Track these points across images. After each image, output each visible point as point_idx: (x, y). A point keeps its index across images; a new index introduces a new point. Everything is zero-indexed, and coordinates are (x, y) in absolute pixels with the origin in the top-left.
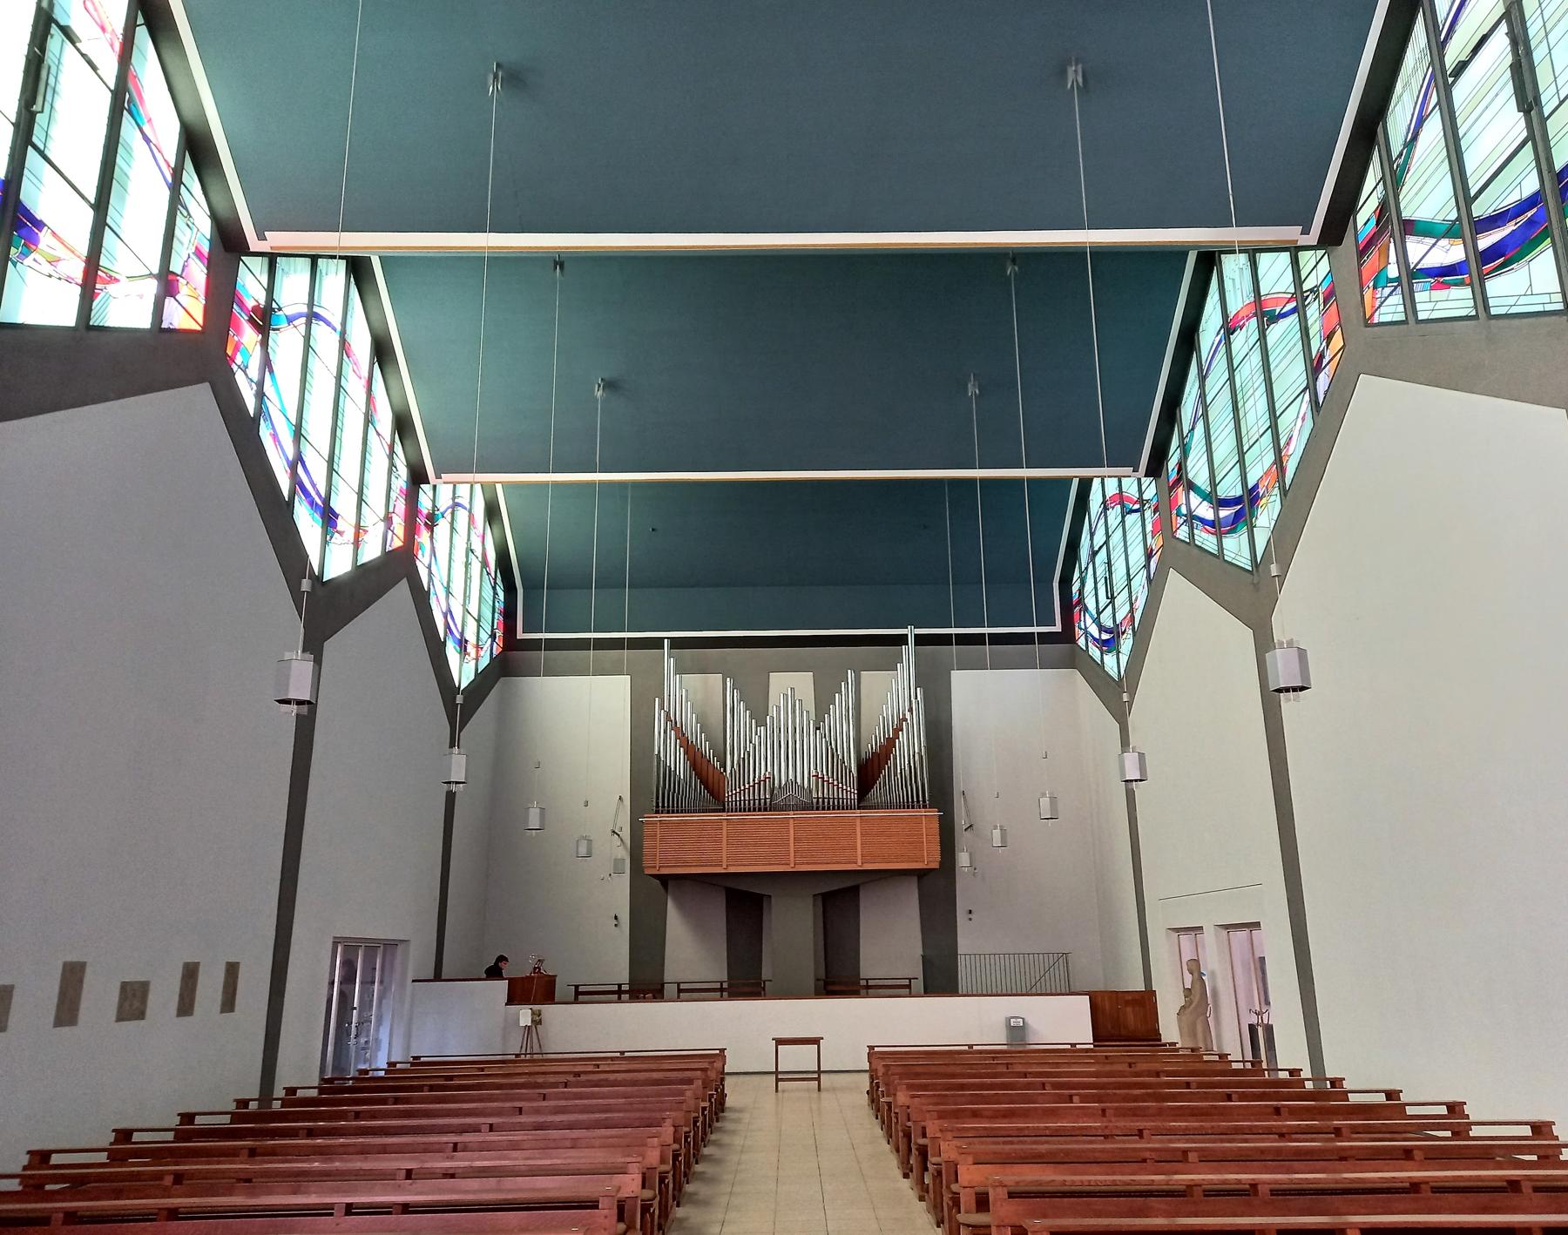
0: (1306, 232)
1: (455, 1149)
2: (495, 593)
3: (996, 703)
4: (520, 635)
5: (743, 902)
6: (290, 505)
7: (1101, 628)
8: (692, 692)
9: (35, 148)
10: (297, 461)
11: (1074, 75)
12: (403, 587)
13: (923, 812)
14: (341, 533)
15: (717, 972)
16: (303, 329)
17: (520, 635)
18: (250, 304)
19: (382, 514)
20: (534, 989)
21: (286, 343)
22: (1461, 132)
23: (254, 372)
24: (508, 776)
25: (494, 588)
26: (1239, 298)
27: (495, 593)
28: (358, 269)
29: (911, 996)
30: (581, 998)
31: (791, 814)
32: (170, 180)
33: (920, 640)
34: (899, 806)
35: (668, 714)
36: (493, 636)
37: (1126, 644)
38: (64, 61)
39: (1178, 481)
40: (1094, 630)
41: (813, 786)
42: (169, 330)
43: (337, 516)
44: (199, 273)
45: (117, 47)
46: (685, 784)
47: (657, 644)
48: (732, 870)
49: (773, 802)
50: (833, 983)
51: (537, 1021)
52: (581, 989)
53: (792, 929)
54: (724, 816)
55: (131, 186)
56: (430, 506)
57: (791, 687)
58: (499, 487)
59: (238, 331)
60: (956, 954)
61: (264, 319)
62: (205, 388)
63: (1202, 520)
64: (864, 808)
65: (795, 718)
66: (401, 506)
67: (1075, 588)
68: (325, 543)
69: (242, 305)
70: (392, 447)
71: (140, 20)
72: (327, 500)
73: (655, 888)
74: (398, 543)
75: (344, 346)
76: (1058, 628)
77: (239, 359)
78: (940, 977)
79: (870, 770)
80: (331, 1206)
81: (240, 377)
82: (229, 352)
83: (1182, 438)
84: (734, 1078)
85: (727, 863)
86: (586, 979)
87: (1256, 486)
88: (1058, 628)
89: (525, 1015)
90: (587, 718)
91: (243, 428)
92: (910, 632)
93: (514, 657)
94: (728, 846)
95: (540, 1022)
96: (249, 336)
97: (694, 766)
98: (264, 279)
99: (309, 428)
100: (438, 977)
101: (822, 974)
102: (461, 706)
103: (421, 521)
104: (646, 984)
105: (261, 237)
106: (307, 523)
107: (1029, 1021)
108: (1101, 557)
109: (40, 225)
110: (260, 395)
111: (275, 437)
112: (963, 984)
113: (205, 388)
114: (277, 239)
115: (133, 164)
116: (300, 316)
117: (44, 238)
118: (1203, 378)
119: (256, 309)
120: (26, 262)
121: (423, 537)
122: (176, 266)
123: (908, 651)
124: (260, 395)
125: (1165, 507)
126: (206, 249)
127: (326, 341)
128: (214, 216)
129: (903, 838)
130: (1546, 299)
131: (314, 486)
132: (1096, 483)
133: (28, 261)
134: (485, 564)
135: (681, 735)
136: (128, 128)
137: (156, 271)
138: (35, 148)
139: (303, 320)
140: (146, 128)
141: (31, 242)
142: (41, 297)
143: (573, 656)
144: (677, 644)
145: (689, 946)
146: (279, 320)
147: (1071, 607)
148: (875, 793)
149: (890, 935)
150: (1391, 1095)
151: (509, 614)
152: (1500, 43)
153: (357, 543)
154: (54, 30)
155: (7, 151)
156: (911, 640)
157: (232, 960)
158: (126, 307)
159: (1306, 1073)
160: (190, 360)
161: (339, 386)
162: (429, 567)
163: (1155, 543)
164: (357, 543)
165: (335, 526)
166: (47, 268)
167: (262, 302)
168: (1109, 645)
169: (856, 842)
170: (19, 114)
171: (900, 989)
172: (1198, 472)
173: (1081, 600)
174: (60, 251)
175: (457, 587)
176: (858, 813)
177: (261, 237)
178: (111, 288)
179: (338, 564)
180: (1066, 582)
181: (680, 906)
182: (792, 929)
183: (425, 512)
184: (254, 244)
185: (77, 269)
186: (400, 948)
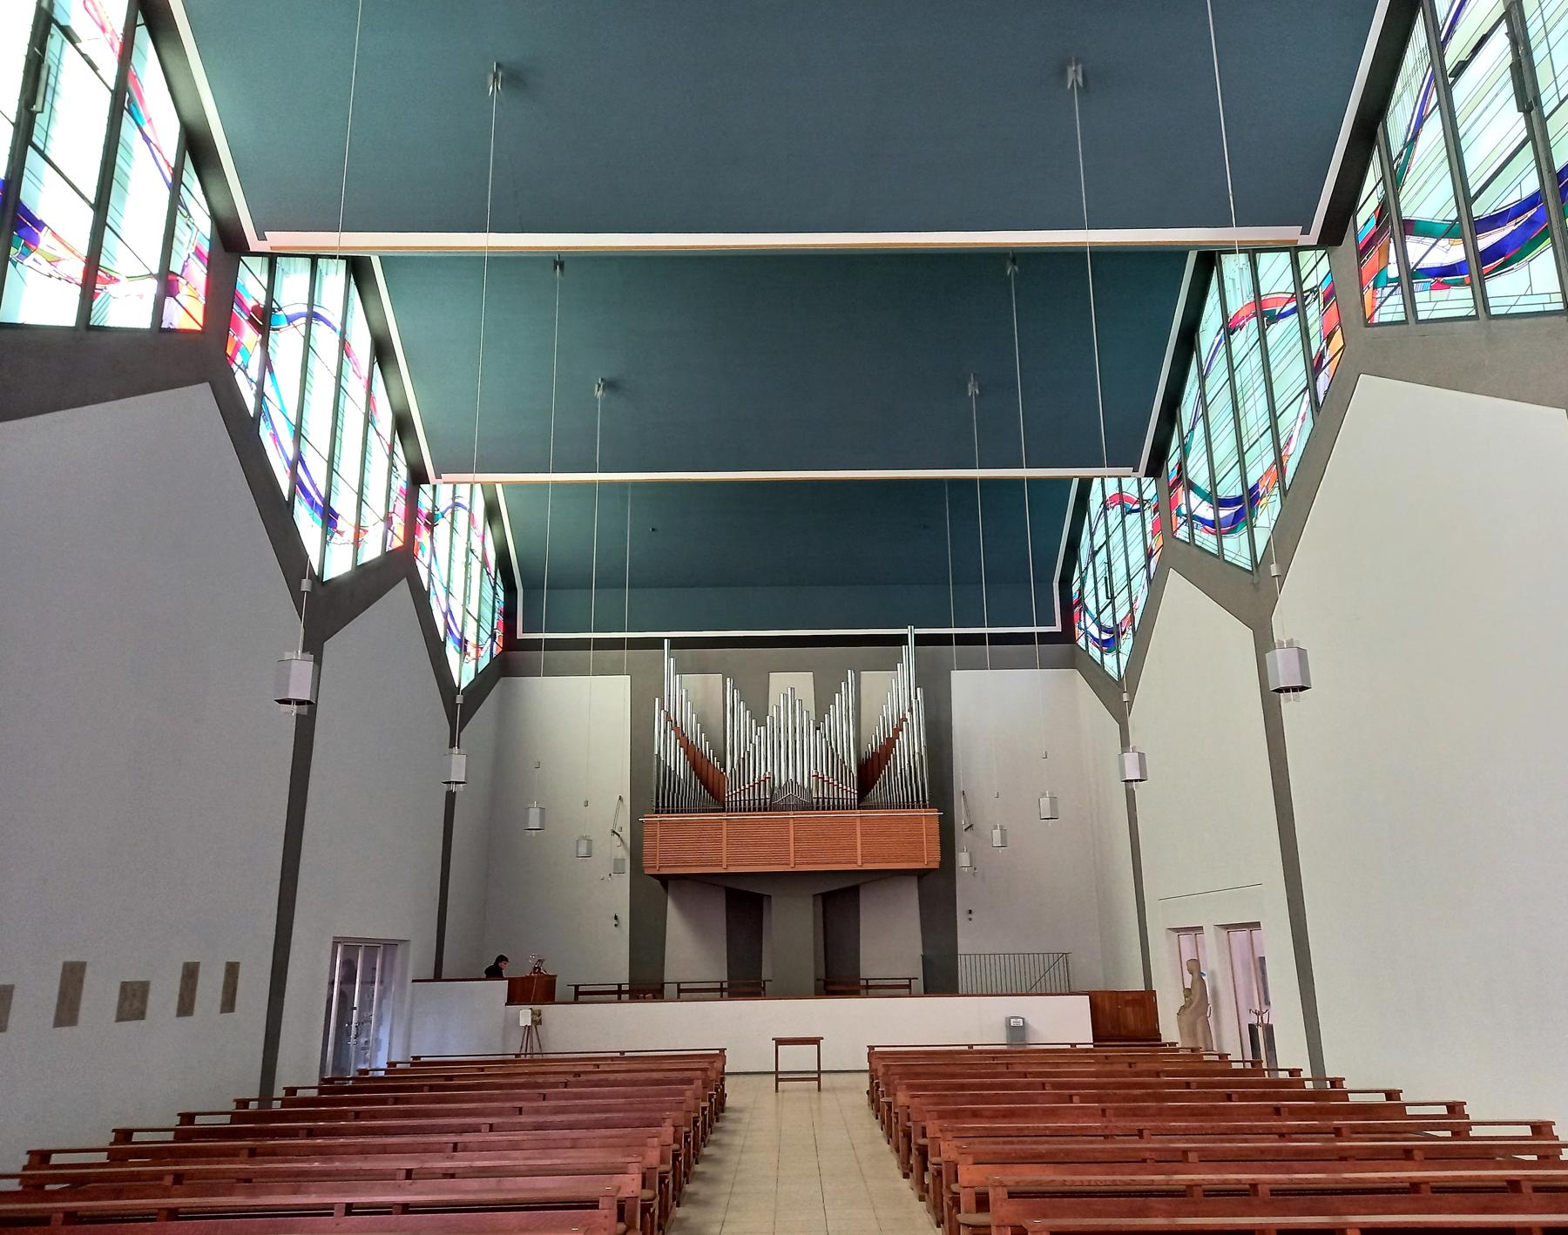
0: (1306, 232)
1: (455, 1149)
2: (495, 593)
3: (996, 703)
4: (520, 635)
5: (743, 902)
6: (290, 505)
7: (1101, 628)
8: (692, 692)
9: (35, 148)
10: (297, 461)
11: (1074, 75)
12: (403, 587)
13: (923, 812)
14: (341, 533)
15: (717, 972)
16: (303, 329)
17: (520, 635)
18: (250, 304)
19: (382, 514)
20: (534, 989)
21: (286, 343)
22: (1461, 132)
23: (254, 372)
24: (508, 776)
25: (494, 588)
26: (1239, 298)
27: (495, 593)
28: (358, 269)
29: (911, 996)
30: (581, 998)
31: (791, 814)
32: (170, 180)
33: (920, 640)
34: (899, 806)
35: (668, 714)
36: (493, 636)
37: (1126, 644)
38: (64, 61)
39: (1178, 481)
40: (1094, 630)
41: (813, 786)
42: (169, 330)
43: (337, 516)
44: (199, 273)
45: (117, 47)
47: (657, 644)
48: (732, 870)
49: (773, 802)
50: (833, 983)
51: (537, 1021)
52: (581, 989)
53: (792, 929)
54: (724, 816)
55: (131, 186)
56: (430, 506)
57: (791, 687)
58: (499, 487)
59: (238, 331)
60: (956, 954)
61: (264, 319)
62: (205, 388)
63: (1202, 520)
64: (864, 808)
65: (795, 718)
66: (401, 506)
67: (1075, 588)
68: (325, 543)
69: (242, 305)
70: (392, 447)
71: (140, 20)
72: (327, 500)
73: (655, 888)
74: (398, 543)
75: (344, 346)
76: (1058, 628)
77: (239, 359)
78: (940, 977)
79: (870, 770)
80: (331, 1206)
81: (240, 377)
82: (229, 352)
83: (1182, 438)
84: (734, 1078)
85: (727, 863)
86: (586, 979)
87: (1256, 486)
88: (1058, 628)
89: (525, 1015)
90: (587, 718)
91: (243, 428)
92: (910, 632)
93: (514, 657)
94: (728, 846)
95: (540, 1022)
96: (249, 336)
97: (694, 766)
98: (264, 279)
99: (309, 428)
100: (438, 977)
101: (822, 974)
102: (461, 706)
103: (421, 521)
104: (646, 984)
105: (261, 237)
106: (307, 523)
107: (1029, 1021)
108: (1101, 557)
109: (40, 225)
110: (260, 395)
111: (275, 437)
112: (963, 984)
113: (205, 388)
114: (277, 239)
115: (133, 164)
116: (300, 316)
117: (44, 238)
118: (1203, 378)
119: (256, 309)
120: (26, 262)
121: (423, 537)
122: (176, 266)
123: (908, 651)
124: (260, 395)
125: (1165, 507)
126: (206, 249)
127: (326, 341)
128: (214, 216)
130: (1546, 299)
131: (314, 486)
132: (1096, 483)
133: (28, 261)
134: (485, 564)
135: (681, 735)
136: (128, 128)
137: (156, 271)
138: (35, 148)
139: (303, 320)
140: (146, 128)
141: (31, 242)
142: (41, 297)
143: (573, 656)
144: (677, 644)
145: (689, 946)
146: (279, 320)
147: (1071, 607)
148: (875, 793)
149: (890, 935)
150: (1391, 1095)
151: (509, 614)
152: (1500, 43)
153: (357, 543)
154: (54, 30)
155: (7, 151)
156: (911, 640)
157: (232, 960)
158: (126, 307)
159: (1306, 1073)
160: (190, 360)
161: (339, 386)
162: (429, 567)
163: (1155, 543)
164: (357, 543)
165: (335, 526)
166: (47, 268)
167: (262, 302)
168: (1109, 645)
169: (856, 842)
170: (19, 114)
171: (900, 989)
172: (1198, 472)
173: (1081, 600)
174: (60, 251)
175: (457, 587)
176: (858, 813)
177: (261, 237)
178: (111, 288)
179: (338, 564)
180: (1066, 582)
181: (680, 906)
182: (792, 929)
183: (425, 512)
184: (254, 244)
185: (77, 269)
186: (400, 948)
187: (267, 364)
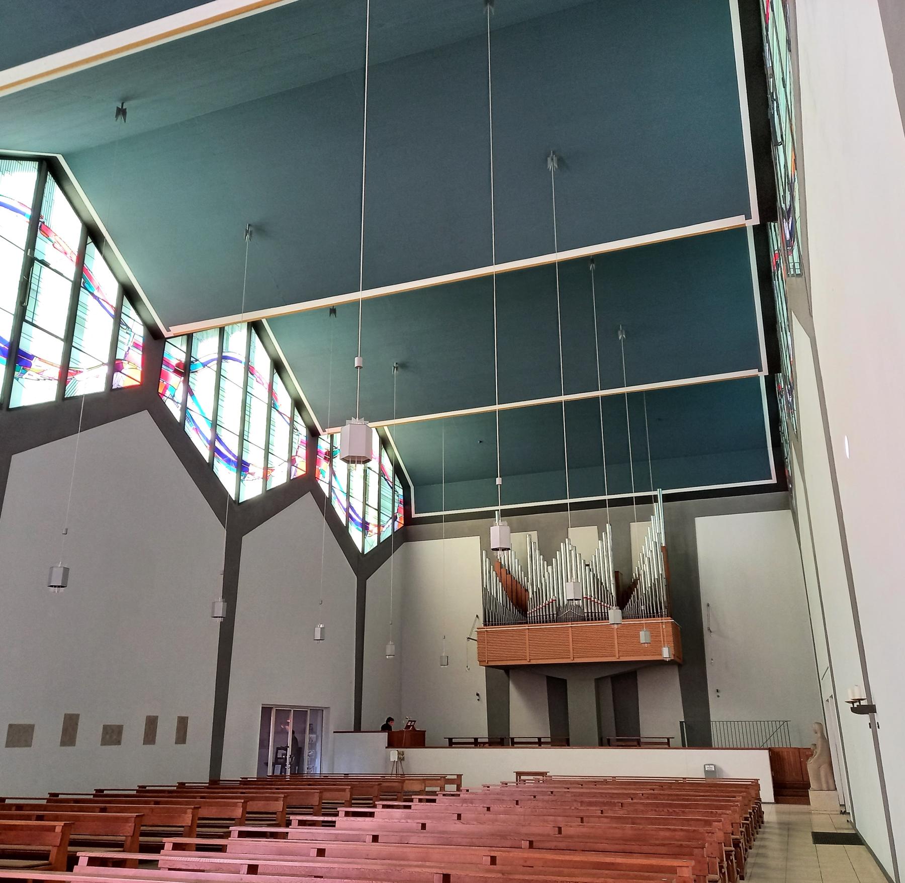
1: (375, 839)
2: (394, 491)
3: (727, 541)
4: (414, 515)
5: (554, 682)
6: (211, 465)
8: (517, 544)
9: (27, 322)
11: (552, 165)
13: (659, 620)
14: (252, 474)
15: (545, 732)
17: (414, 515)
18: (174, 362)
19: (286, 457)
20: (418, 739)
21: (203, 380)
23: (179, 397)
24: (410, 602)
27: (394, 491)
28: (256, 326)
29: (669, 748)
32: (113, 313)
33: (667, 498)
36: (394, 518)
38: (44, 279)
42: (117, 389)
43: (248, 465)
44: (137, 356)
45: (75, 259)
46: (513, 602)
48: (533, 662)
49: (559, 615)
51: (401, 759)
52: (454, 740)
53: (582, 702)
54: (526, 627)
55: (87, 324)
56: (328, 447)
58: (386, 428)
59: (166, 378)
60: (709, 721)
61: (185, 370)
62: (145, 414)
65: (578, 558)
66: (303, 452)
68: (239, 481)
69: (168, 365)
73: (503, 675)
74: (300, 473)
75: (249, 369)
76: (774, 481)
77: (168, 393)
78: (697, 735)
80: (37, 820)
81: (169, 404)
82: (160, 391)
86: (458, 734)
89: (394, 754)
90: (456, 567)
92: (659, 493)
93: (409, 531)
94: (532, 645)
95: (403, 759)
96: (175, 381)
98: (184, 348)
99: (223, 419)
100: (358, 728)
102: (364, 565)
103: (321, 457)
104: (500, 739)
105: (169, 330)
106: (225, 475)
107: (719, 764)
109: (31, 357)
110: (185, 409)
111: (197, 429)
112: (715, 741)
113: (145, 414)
114: (175, 330)
115: (88, 312)
116: (213, 360)
117: (35, 362)
119: (178, 365)
120: (24, 376)
121: (324, 466)
122: (120, 355)
123: (658, 508)
124: (185, 409)
126: (140, 341)
127: (234, 371)
128: (145, 324)
129: (654, 639)
131: (230, 452)
133: (26, 376)
136: (84, 296)
137: (106, 360)
138: (27, 322)
139: (215, 362)
140: (96, 293)
141: (28, 365)
142: (34, 391)
143: (457, 525)
144: (504, 513)
145: (524, 715)
146: (197, 366)
149: (661, 708)
151: (406, 502)
153: (266, 478)
155: (11, 328)
156: (660, 499)
157: (153, 714)
158: (89, 382)
160: (146, 398)
161: (246, 392)
162: (330, 484)
164: (266, 478)
165: (247, 470)
166: (39, 377)
167: (183, 360)
170: (17, 309)
171: (667, 744)
174: (44, 366)
177: (169, 330)
178: (77, 377)
179: (251, 490)
181: (519, 687)
182: (582, 702)
183: (324, 451)
184: (166, 334)
185: (55, 373)
186: (320, 713)
187: (189, 391)
